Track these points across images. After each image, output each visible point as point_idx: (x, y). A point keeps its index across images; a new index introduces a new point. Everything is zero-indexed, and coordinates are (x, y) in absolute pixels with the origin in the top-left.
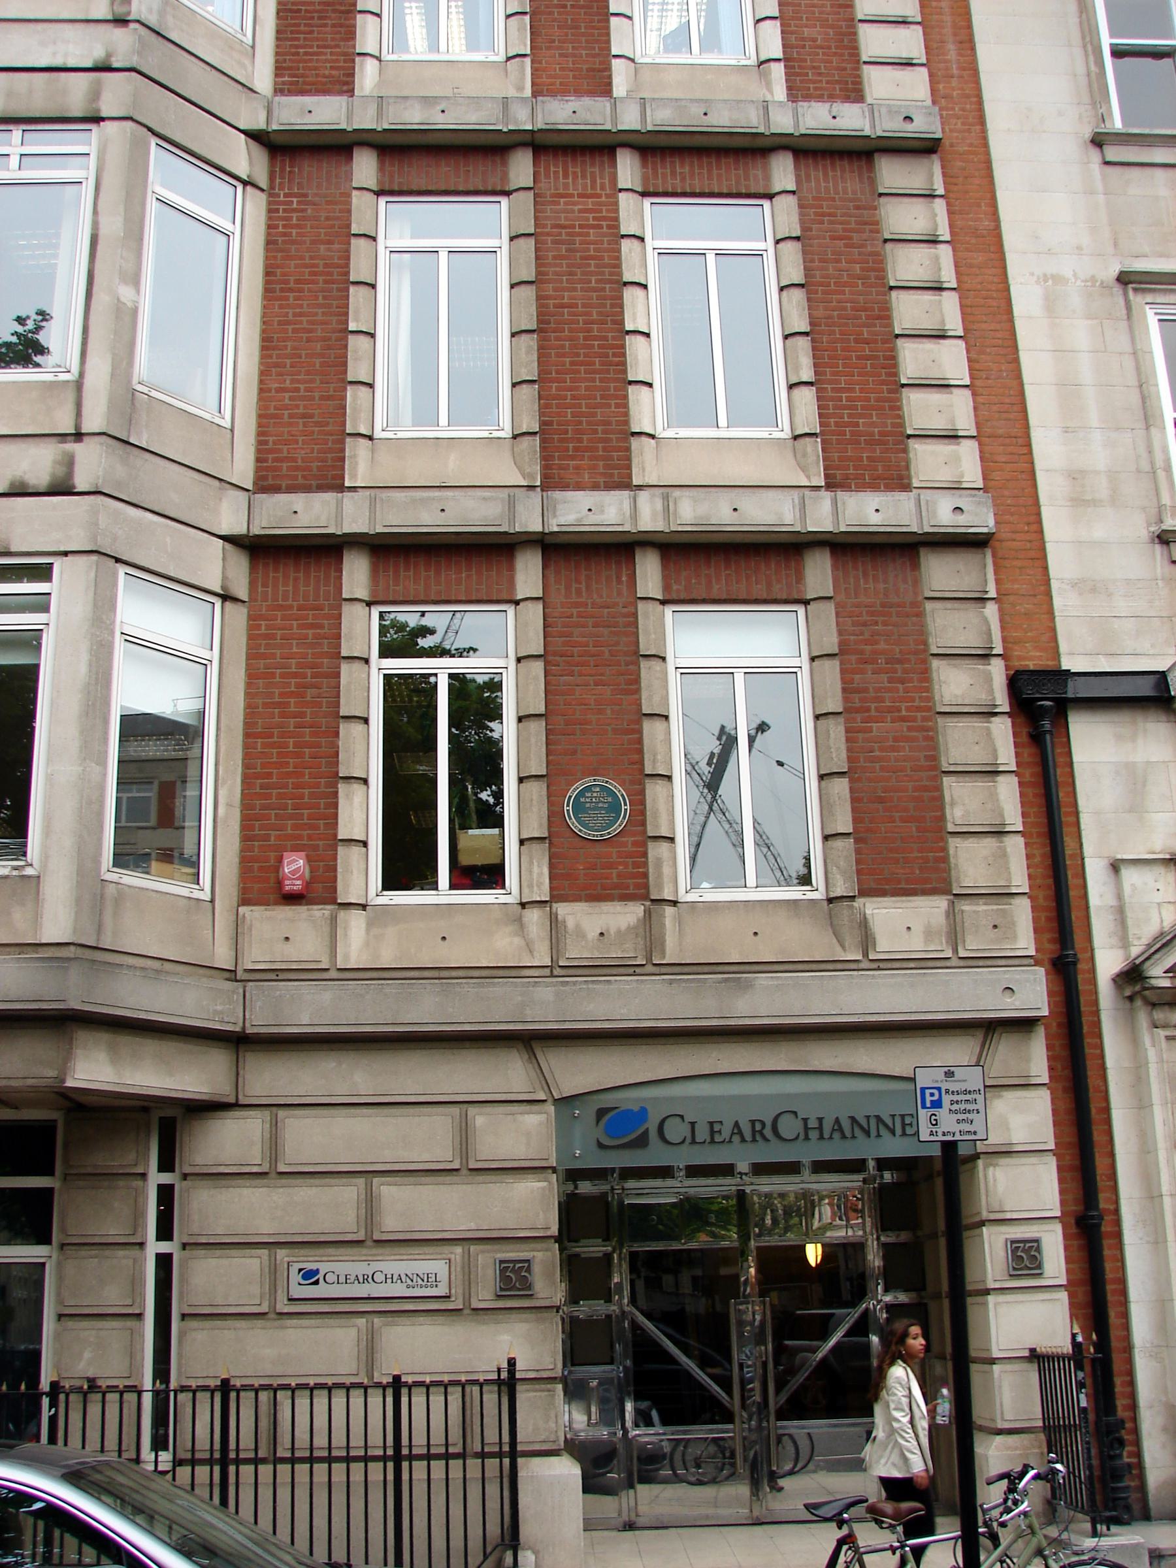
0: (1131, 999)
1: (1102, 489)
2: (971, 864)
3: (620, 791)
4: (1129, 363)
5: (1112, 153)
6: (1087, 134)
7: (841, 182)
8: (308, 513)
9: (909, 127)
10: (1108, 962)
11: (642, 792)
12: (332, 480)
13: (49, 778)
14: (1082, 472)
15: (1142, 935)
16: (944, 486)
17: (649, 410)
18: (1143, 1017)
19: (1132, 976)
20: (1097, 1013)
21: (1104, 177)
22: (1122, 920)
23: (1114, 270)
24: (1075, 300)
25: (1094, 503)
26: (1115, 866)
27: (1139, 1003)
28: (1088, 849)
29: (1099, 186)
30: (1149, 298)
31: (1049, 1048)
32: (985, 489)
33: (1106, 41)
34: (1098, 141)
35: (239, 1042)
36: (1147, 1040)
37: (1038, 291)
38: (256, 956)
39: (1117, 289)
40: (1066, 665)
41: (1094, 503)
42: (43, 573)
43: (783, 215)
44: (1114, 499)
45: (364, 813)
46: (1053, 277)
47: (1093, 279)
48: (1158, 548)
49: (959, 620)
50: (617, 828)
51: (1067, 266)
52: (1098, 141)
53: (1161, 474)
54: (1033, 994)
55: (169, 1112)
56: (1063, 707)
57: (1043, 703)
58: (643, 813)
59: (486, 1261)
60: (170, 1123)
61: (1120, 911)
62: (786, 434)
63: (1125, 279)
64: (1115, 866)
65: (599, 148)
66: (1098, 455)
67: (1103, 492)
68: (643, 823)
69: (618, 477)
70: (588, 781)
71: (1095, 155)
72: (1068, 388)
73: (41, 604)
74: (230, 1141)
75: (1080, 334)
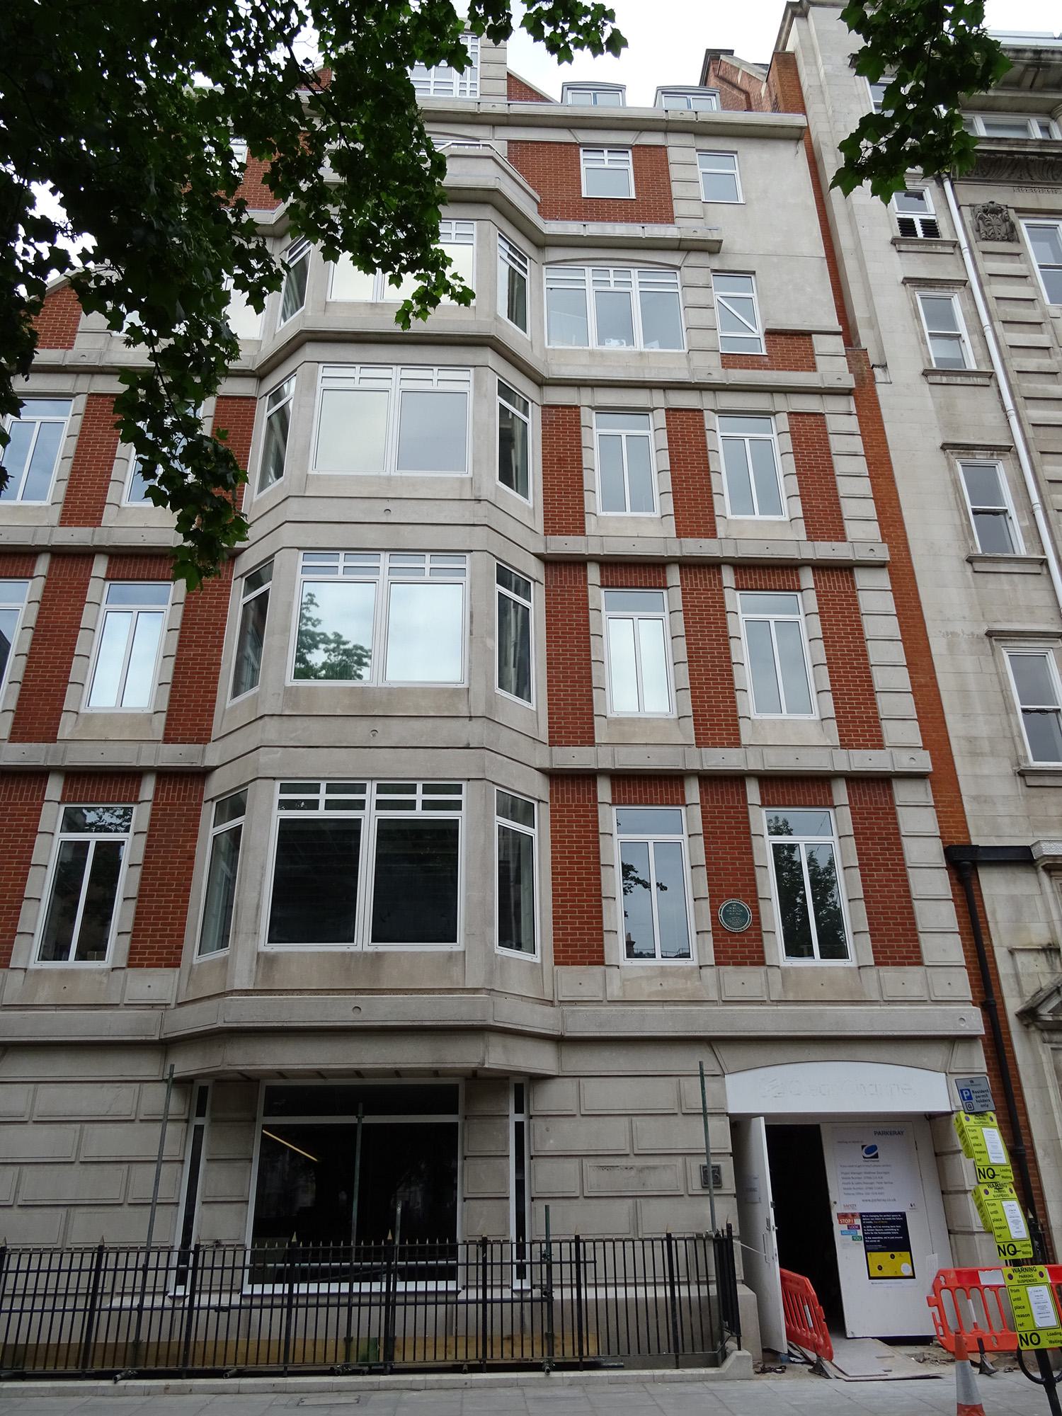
0: (1027, 1026)
1: (986, 747)
2: (931, 947)
3: (746, 906)
4: (995, 678)
5: (978, 566)
6: (964, 556)
7: (835, 583)
8: (575, 757)
9: (872, 554)
10: (1013, 1006)
11: (757, 907)
12: (588, 739)
13: (468, 898)
14: (975, 738)
15: (1030, 989)
16: (902, 746)
17: (747, 704)
18: (1036, 1037)
19: (1029, 1016)
20: (1009, 1033)
21: (974, 579)
22: (1021, 980)
23: (986, 628)
24: (964, 646)
25: (982, 754)
26: (1012, 952)
27: (1033, 1028)
28: (995, 942)
29: (972, 584)
30: (1003, 644)
31: (985, 1052)
32: (924, 749)
33: (970, 507)
34: (970, 560)
35: (560, 1041)
36: (1040, 1050)
37: (944, 641)
38: (564, 994)
39: (986, 640)
40: (975, 841)
41: (982, 754)
42: (458, 790)
43: (810, 600)
44: (993, 753)
45: (127, 882)
46: (952, 633)
47: (972, 634)
48: (1018, 778)
49: (917, 820)
50: (746, 927)
51: (958, 627)
52: (970, 560)
53: (1017, 739)
54: (974, 1021)
55: (519, 1080)
56: (975, 865)
57: (965, 863)
58: (759, 918)
59: (696, 1164)
60: (522, 1087)
61: (1017, 976)
62: (817, 718)
63: (990, 634)
64: (1012, 952)
65: (712, 565)
66: (983, 728)
67: (986, 748)
68: (759, 924)
69: (580, 529)
70: (730, 901)
71: (968, 567)
72: (964, 692)
73: (457, 805)
74: (549, 1098)
75: (968, 663)
